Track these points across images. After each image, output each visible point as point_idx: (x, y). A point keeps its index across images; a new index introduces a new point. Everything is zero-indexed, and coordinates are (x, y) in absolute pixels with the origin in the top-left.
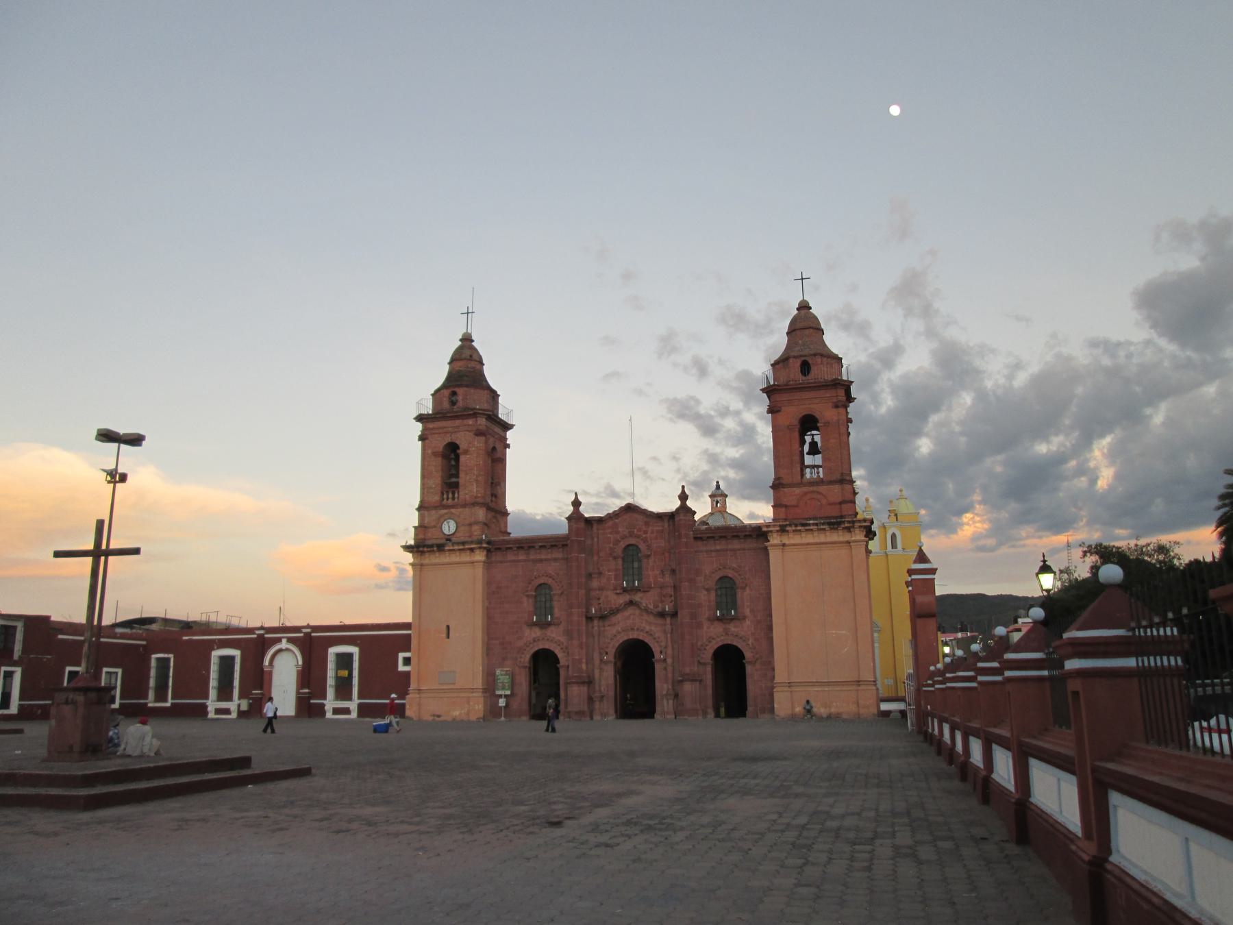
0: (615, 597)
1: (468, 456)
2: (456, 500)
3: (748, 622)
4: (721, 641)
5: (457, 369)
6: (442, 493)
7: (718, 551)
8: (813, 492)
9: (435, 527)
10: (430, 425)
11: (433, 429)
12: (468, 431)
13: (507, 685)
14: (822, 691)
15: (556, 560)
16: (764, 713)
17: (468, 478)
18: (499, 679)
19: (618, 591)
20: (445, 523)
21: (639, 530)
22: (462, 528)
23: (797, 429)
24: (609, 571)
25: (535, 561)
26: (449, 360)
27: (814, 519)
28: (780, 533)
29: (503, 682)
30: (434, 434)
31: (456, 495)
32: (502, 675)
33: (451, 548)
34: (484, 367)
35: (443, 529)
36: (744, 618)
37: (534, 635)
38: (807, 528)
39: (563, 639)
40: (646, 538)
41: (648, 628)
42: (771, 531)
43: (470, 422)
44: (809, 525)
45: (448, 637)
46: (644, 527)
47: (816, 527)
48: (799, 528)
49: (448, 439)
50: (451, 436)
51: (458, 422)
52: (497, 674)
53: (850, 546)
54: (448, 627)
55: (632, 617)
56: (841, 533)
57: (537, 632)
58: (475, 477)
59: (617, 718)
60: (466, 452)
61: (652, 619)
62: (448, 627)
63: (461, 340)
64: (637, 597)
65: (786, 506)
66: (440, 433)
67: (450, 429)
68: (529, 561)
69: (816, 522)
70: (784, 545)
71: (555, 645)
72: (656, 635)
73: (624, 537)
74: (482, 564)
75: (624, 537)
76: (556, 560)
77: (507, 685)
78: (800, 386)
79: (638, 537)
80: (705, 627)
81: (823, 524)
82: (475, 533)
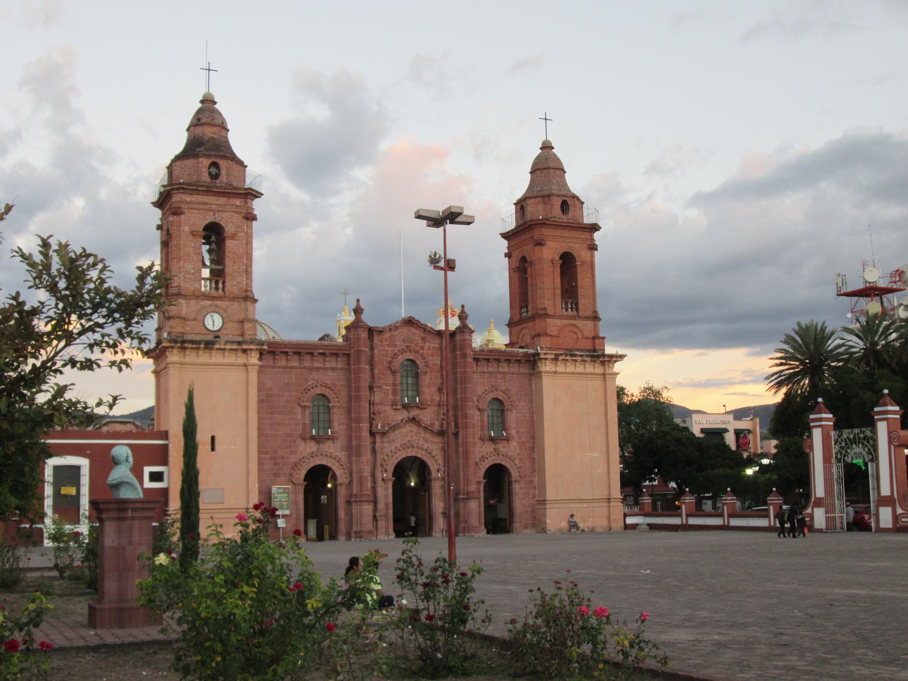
0: (393, 412)
1: (236, 242)
2: (220, 291)
3: (514, 444)
4: (493, 460)
5: (209, 135)
7: (490, 373)
8: (572, 325)
9: (195, 319)
11: (191, 202)
12: (234, 212)
13: (285, 504)
14: (581, 507)
15: (333, 369)
16: (527, 528)
17: (236, 267)
18: (276, 498)
20: (208, 316)
21: (417, 345)
22: (230, 325)
23: (559, 264)
24: (386, 385)
25: (311, 369)
26: (529, 170)
27: (582, 350)
28: (179, 350)
29: (281, 501)
30: (192, 209)
31: (220, 285)
32: (278, 493)
33: (222, 347)
34: (229, 134)
35: (206, 323)
37: (309, 451)
38: (574, 358)
39: (342, 455)
40: (423, 353)
41: (425, 447)
43: (238, 202)
44: (575, 355)
45: (213, 449)
46: (420, 342)
47: (580, 358)
48: (567, 358)
49: (210, 218)
50: (214, 215)
51: (222, 200)
52: (273, 492)
53: (247, 369)
54: (213, 438)
55: (409, 434)
56: (597, 365)
57: (312, 447)
58: (244, 267)
59: (488, 532)
60: (233, 237)
61: (428, 436)
62: (213, 438)
63: (541, 149)
64: (415, 412)
66: (200, 209)
67: (214, 206)
68: (304, 368)
69: (582, 353)
71: (333, 461)
72: (434, 453)
73: (402, 352)
74: (257, 368)
75: (402, 352)
76: (333, 369)
77: (285, 504)
78: (564, 224)
79: (416, 352)
80: (478, 447)
81: (587, 356)
82: (248, 333)
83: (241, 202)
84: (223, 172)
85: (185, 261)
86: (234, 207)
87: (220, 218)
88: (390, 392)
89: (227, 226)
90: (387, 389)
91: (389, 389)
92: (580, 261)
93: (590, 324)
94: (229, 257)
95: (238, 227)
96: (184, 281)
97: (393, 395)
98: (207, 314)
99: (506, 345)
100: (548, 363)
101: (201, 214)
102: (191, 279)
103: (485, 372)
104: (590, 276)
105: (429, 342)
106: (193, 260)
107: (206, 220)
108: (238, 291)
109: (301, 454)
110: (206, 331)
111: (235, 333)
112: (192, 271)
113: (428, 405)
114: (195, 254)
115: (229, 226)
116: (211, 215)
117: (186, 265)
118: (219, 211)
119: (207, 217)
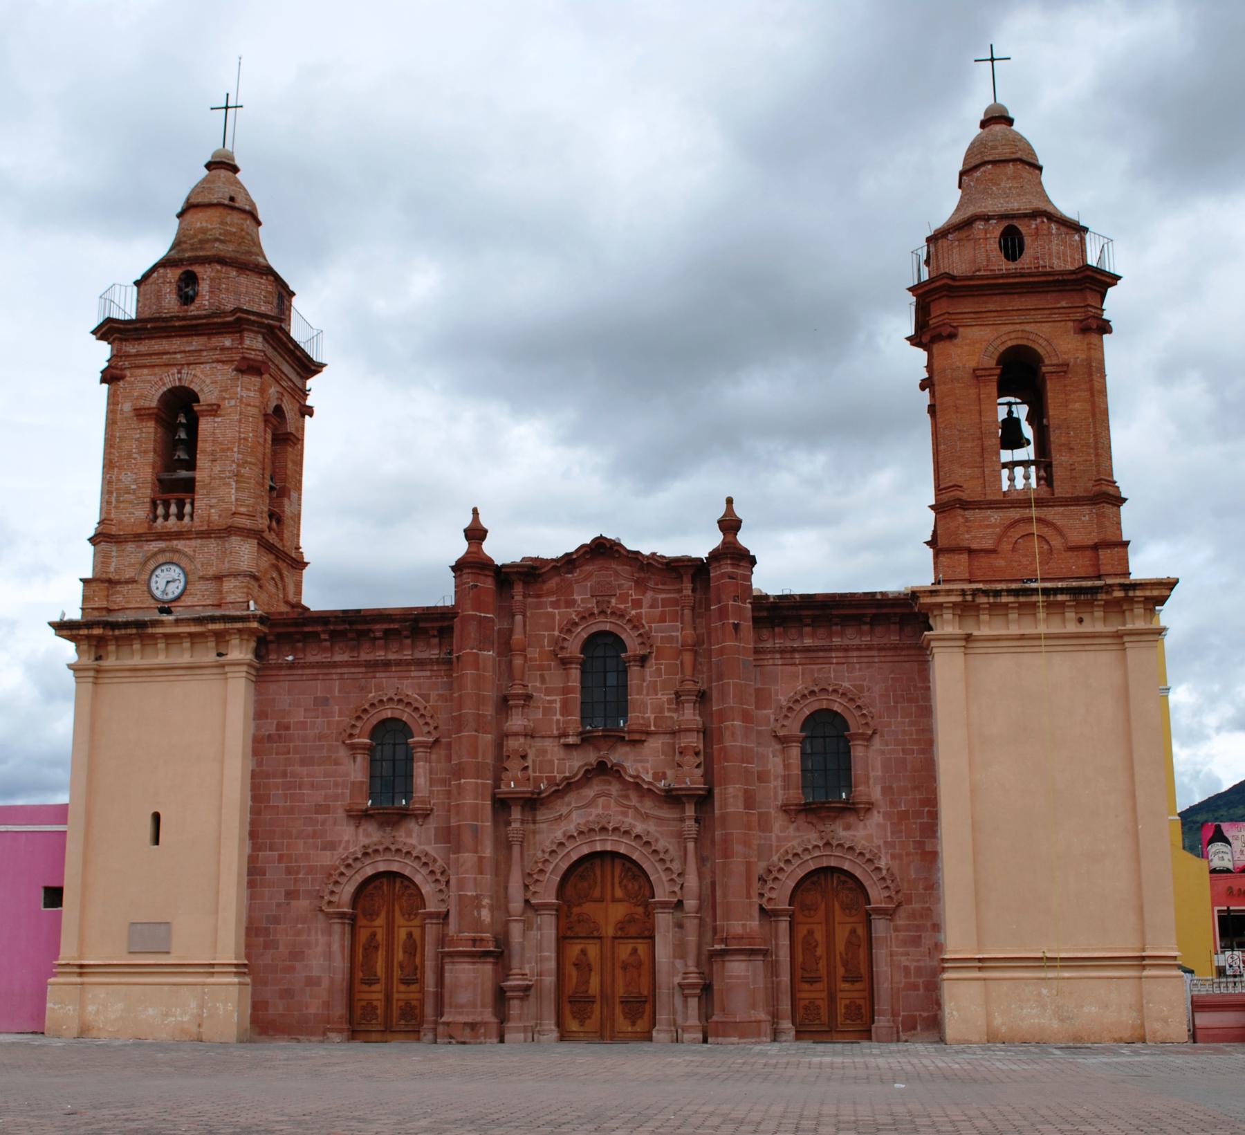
2: (187, 519)
3: (876, 818)
6: (154, 504)
7: (807, 650)
10: (132, 348)
12: (218, 361)
17: (217, 469)
19: (571, 740)
24: (548, 692)
30: (138, 367)
31: (188, 508)
36: (869, 807)
40: (639, 616)
42: (940, 606)
49: (171, 379)
50: (179, 372)
51: (196, 343)
60: (214, 410)
61: (648, 806)
65: (970, 551)
66: (153, 366)
67: (178, 356)
70: (968, 638)
75: (586, 616)
83: (233, 340)
84: (204, 287)
85: (120, 468)
86: (218, 352)
87: (190, 378)
88: (558, 705)
89: (202, 390)
90: (550, 702)
91: (555, 701)
92: (1055, 361)
93: (1085, 514)
94: (204, 451)
95: (225, 391)
96: (116, 507)
97: (562, 715)
98: (156, 568)
99: (933, 584)
100: (948, 616)
101: (155, 375)
102: (131, 502)
103: (794, 650)
104: (1086, 394)
105: (654, 590)
106: (136, 464)
107: (164, 384)
108: (220, 516)
109: (346, 848)
110: (153, 601)
111: (208, 602)
112: (134, 487)
113: (649, 733)
114: (139, 453)
115: (206, 390)
116: (173, 374)
117: (122, 477)
118: (189, 364)
119: (166, 380)
